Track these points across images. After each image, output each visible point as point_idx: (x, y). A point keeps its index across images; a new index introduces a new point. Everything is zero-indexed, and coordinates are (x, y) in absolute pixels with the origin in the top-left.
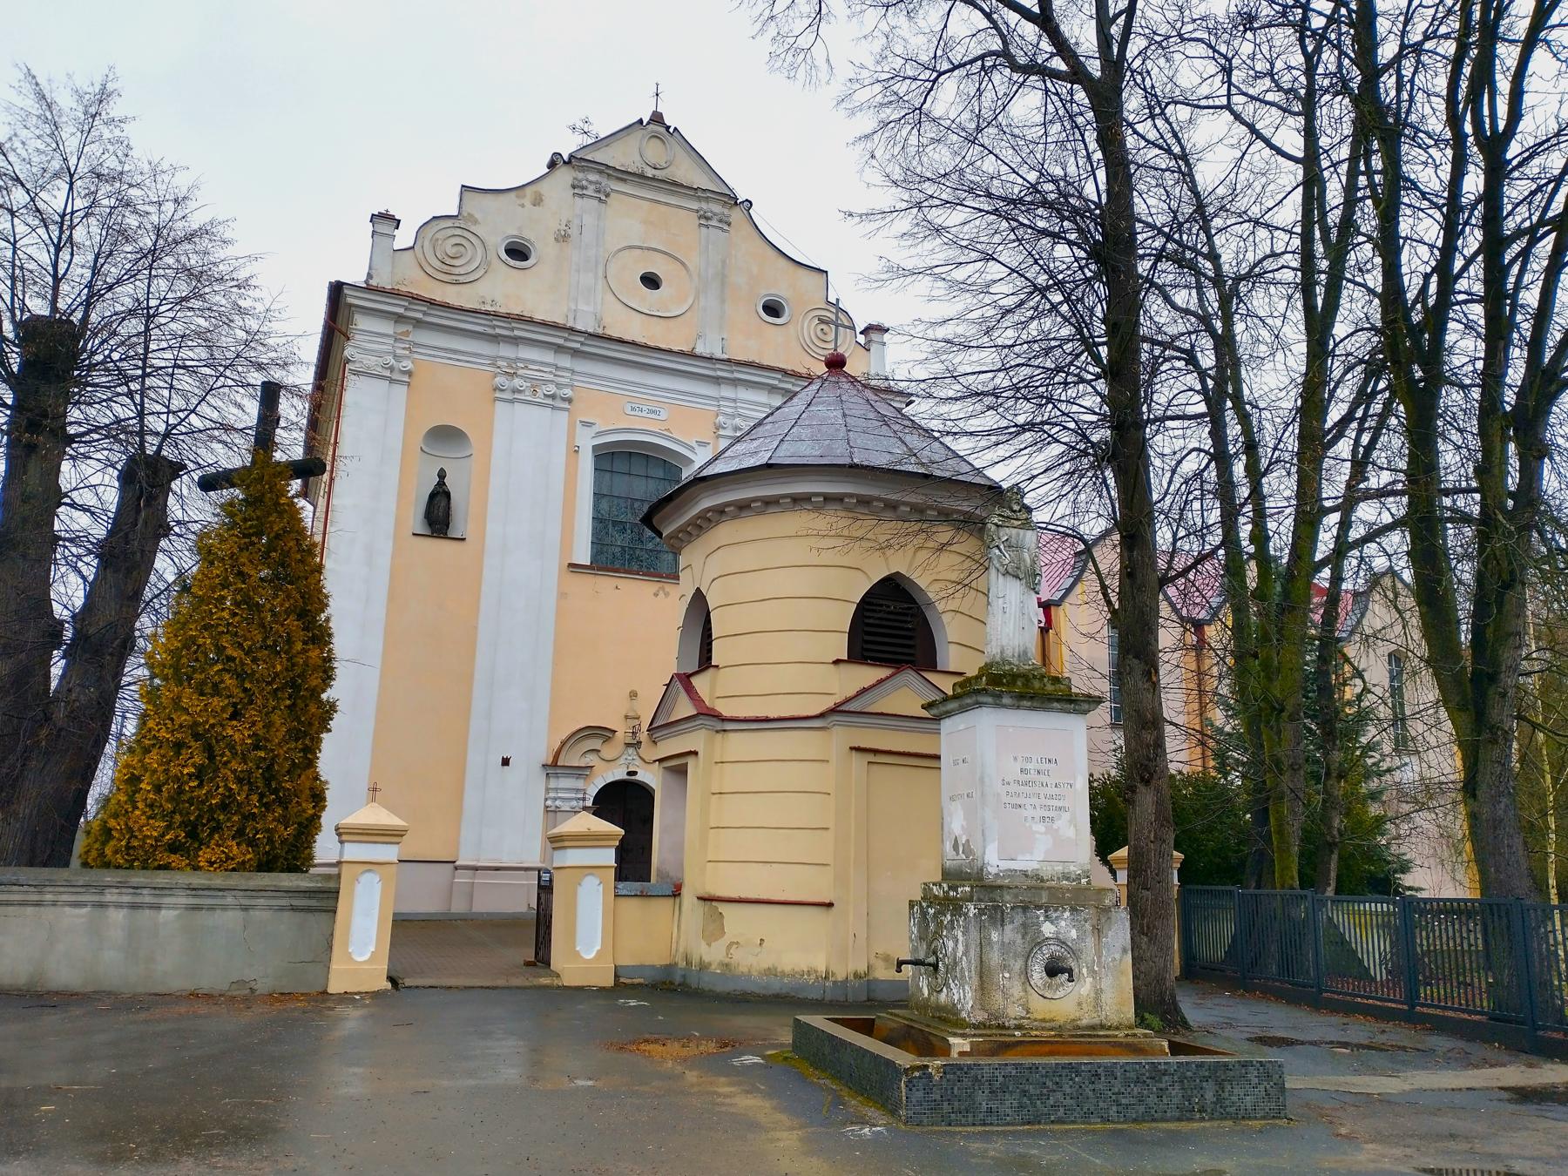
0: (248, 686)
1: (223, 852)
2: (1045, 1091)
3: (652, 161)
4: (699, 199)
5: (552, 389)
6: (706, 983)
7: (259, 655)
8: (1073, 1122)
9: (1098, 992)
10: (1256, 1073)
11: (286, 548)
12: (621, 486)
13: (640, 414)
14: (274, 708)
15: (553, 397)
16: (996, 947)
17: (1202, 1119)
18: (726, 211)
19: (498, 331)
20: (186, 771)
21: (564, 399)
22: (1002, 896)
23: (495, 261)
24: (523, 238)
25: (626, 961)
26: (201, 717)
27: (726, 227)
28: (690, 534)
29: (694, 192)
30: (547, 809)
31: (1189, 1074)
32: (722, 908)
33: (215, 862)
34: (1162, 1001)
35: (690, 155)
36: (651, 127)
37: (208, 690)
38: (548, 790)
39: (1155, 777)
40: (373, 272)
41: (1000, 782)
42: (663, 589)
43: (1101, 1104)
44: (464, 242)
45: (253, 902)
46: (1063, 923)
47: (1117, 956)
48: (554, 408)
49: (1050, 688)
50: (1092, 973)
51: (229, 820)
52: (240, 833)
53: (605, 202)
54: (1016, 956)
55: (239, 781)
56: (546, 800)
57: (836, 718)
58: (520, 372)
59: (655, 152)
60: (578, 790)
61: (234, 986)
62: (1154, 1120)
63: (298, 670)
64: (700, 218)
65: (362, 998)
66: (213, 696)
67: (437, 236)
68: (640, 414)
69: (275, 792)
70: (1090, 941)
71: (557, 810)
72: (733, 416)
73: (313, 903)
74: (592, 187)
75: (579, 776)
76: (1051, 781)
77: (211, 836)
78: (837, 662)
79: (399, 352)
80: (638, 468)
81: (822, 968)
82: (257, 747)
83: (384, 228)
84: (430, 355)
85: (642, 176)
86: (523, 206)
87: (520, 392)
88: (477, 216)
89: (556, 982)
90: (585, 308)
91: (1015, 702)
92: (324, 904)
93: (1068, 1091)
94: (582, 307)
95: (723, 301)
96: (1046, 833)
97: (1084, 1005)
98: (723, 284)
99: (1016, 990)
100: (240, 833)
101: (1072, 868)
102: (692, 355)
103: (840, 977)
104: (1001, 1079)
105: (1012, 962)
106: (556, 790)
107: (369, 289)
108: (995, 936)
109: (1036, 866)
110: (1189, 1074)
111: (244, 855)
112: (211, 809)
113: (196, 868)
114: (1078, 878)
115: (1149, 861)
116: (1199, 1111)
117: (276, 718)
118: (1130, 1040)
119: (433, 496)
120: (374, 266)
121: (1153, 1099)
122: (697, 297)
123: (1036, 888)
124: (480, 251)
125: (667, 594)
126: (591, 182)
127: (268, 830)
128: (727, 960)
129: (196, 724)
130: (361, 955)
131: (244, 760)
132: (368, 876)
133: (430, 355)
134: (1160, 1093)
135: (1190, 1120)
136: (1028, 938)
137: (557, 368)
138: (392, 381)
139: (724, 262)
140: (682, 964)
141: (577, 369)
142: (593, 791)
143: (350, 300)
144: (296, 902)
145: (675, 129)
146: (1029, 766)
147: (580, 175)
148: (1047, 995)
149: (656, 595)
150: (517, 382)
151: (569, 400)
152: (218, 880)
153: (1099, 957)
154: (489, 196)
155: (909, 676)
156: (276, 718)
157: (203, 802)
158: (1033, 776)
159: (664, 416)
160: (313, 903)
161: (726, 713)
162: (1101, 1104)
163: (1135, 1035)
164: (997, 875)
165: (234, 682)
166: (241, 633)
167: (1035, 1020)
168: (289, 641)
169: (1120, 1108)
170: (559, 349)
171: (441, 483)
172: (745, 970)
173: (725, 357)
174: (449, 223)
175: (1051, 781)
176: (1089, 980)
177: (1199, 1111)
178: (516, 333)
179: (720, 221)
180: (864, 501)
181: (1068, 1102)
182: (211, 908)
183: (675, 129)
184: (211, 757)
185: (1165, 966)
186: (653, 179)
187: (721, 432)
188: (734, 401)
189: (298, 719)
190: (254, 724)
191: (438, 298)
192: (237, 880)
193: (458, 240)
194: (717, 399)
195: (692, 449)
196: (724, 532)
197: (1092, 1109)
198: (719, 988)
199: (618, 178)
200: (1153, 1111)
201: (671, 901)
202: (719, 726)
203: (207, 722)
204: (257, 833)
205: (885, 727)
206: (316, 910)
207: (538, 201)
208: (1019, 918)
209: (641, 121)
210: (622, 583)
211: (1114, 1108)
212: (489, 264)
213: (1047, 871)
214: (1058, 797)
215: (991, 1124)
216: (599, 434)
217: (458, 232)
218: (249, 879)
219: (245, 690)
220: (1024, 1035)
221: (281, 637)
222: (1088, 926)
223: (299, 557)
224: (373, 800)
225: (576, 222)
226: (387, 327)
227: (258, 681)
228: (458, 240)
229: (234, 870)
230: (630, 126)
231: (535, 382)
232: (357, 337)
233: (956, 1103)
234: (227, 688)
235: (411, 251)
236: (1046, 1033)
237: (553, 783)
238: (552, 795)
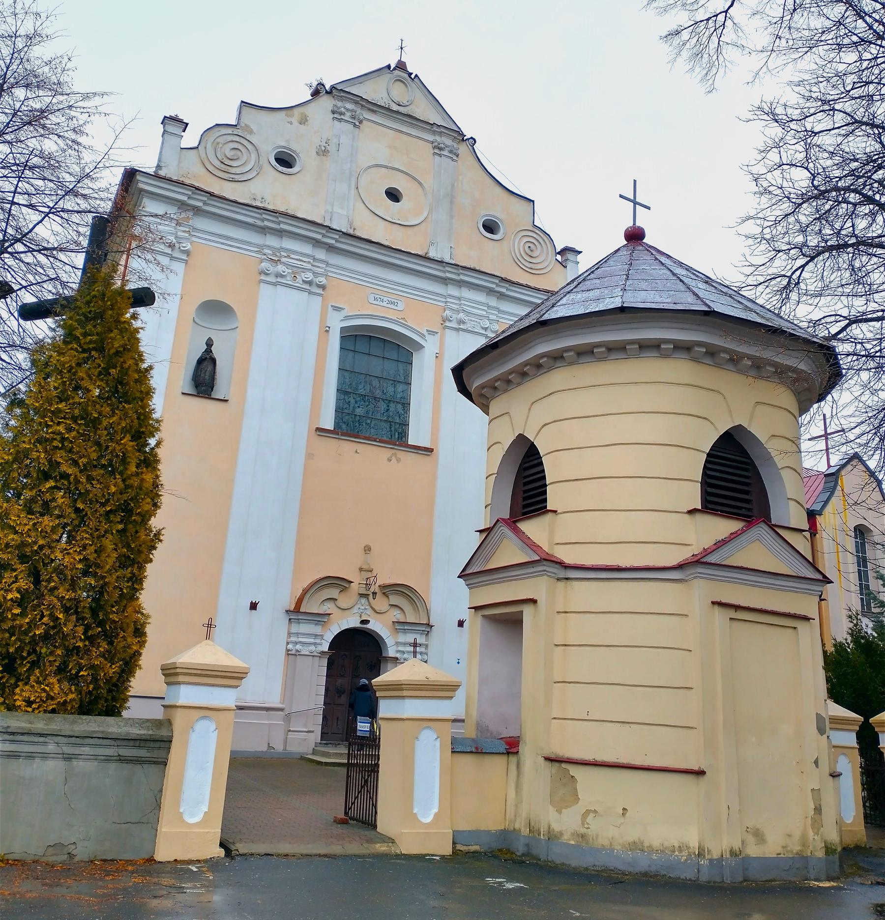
0: (80, 506)
1: (44, 690)
3: (396, 99)
4: (434, 133)
5: (310, 276)
6: (557, 856)
7: (94, 473)
11: (126, 366)
12: (362, 364)
13: (381, 303)
14: (106, 532)
15: (310, 283)
18: (455, 145)
19: (266, 223)
20: (10, 596)
21: (319, 286)
23: (266, 166)
24: (290, 149)
25: (464, 826)
26: (30, 536)
27: (455, 158)
28: (495, 388)
29: (430, 126)
30: (288, 653)
32: (574, 770)
33: (34, 702)
35: (427, 98)
36: (397, 72)
37: (37, 508)
38: (289, 634)
42: (395, 455)
44: (240, 147)
45: (77, 751)
48: (310, 293)
51: (52, 653)
52: (61, 670)
53: (358, 127)
55: (66, 610)
56: (288, 643)
57: (700, 570)
58: (283, 260)
59: (399, 93)
60: (316, 636)
61: (51, 849)
63: (131, 493)
64: (434, 148)
65: (201, 871)
66: (42, 515)
67: (218, 140)
68: (381, 303)
69: (101, 624)
71: (297, 654)
72: (458, 312)
73: (142, 753)
74: (348, 114)
75: (318, 623)
77: (30, 671)
78: (691, 512)
80: (376, 349)
81: (694, 844)
82: (86, 573)
83: (173, 128)
84: (206, 239)
85: (388, 109)
86: (291, 123)
87: (282, 276)
88: (254, 127)
89: (394, 850)
90: (340, 211)
92: (156, 754)
94: (337, 209)
95: (451, 217)
98: (452, 202)
100: (61, 670)
102: (426, 258)
103: (716, 855)
106: (297, 634)
107: (156, 176)
111: (67, 695)
112: (34, 641)
113: (11, 708)
117: (108, 543)
119: (200, 361)
120: (164, 159)
122: (430, 212)
124: (254, 156)
125: (398, 460)
126: (348, 110)
127: (92, 667)
128: (583, 831)
129: (23, 544)
131: (73, 586)
132: (204, 723)
133: (206, 239)
137: (315, 259)
139: (453, 186)
140: (525, 832)
141: (330, 262)
142: (329, 637)
143: (141, 186)
144: (125, 752)
145: (416, 76)
147: (339, 104)
149: (389, 460)
150: (280, 268)
151: (323, 287)
152: (40, 723)
154: (264, 113)
156: (108, 543)
157: (26, 633)
159: (401, 306)
160: (142, 753)
161: (568, 560)
165: (66, 501)
166: (76, 449)
168: (124, 461)
170: (317, 243)
171: (208, 351)
172: (606, 843)
173: (453, 262)
178: (283, 226)
179: (451, 152)
180: (712, 353)
182: (30, 756)
183: (416, 76)
184: (37, 582)
186: (397, 112)
187: (448, 324)
188: (459, 299)
189: (128, 546)
190: (84, 547)
191: (216, 192)
192: (61, 723)
193: (236, 145)
194: (445, 297)
195: (422, 336)
196: (559, 378)
198: (574, 862)
199: (370, 109)
201: (502, 760)
202: (562, 573)
203: (35, 543)
204: (81, 669)
205: (743, 582)
206: (145, 762)
207: (303, 121)
209: (389, 67)
210: (361, 448)
212: (261, 168)
216: (347, 318)
218: (74, 722)
219: (77, 510)
221: (117, 456)
223: (136, 376)
224: (208, 637)
225: (334, 141)
227: (91, 502)
228: (236, 145)
229: (53, 711)
230: (381, 69)
231: (295, 269)
234: (59, 507)
237: (295, 628)
238: (293, 639)
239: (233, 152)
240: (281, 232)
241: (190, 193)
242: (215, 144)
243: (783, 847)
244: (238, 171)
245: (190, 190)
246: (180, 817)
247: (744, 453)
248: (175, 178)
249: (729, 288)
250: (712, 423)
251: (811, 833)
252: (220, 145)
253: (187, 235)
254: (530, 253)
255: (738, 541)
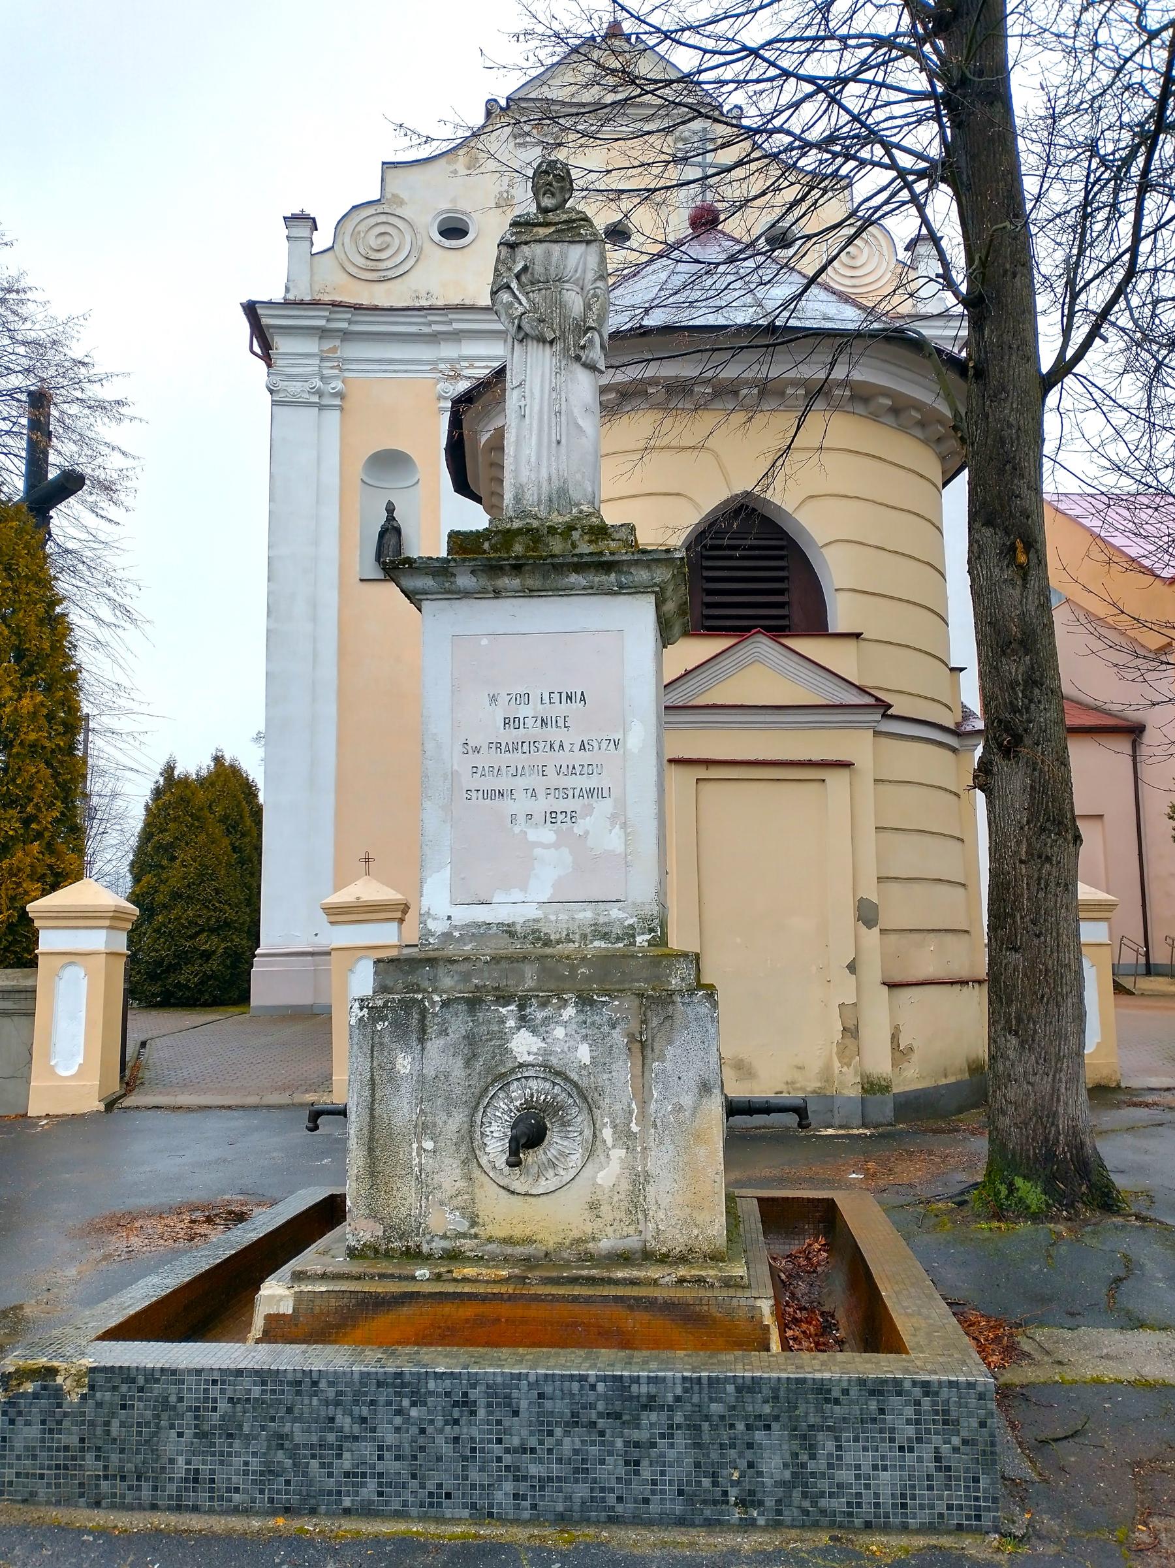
2: (331, 1438)
8: (399, 1515)
9: (639, 1181)
10: (909, 1412)
16: (405, 1087)
17: (748, 1525)
22: (433, 980)
23: (428, 246)
24: (457, 211)
31: (716, 1408)
34: (1050, 1156)
39: (1027, 741)
40: (291, 285)
41: (459, 748)
43: (474, 1476)
46: (559, 1032)
47: (687, 1100)
49: (584, 548)
50: (625, 1136)
54: (450, 1104)
62: (614, 1520)
67: (359, 228)
70: (623, 1070)
76: (571, 738)
79: (326, 372)
83: (302, 231)
88: (404, 195)
91: (484, 581)
93: (390, 1439)
96: (556, 845)
97: (605, 1209)
99: (449, 1177)
101: (615, 913)
104: (223, 1406)
105: (440, 1118)
107: (287, 303)
108: (404, 1064)
109: (532, 912)
110: (716, 1408)
114: (630, 934)
115: (1019, 896)
116: (742, 1503)
118: (687, 1294)
119: (382, 535)
121: (613, 1468)
123: (511, 959)
130: (67, 1069)
134: (635, 1454)
135: (710, 1524)
136: (479, 1065)
138: (322, 407)
146: (523, 711)
148: (517, 1186)
153: (644, 1104)
155: (762, 646)
158: (532, 731)
162: (474, 1476)
163: (700, 1280)
164: (447, 936)
167: (490, 1240)
169: (523, 1488)
171: (391, 518)
174: (371, 211)
175: (571, 738)
176: (618, 1154)
177: (742, 1503)
178: (456, 326)
180: (678, 389)
181: (389, 1465)
185: (1055, 1091)
193: (382, 229)
197: (449, 1485)
200: (611, 1499)
206: (14, 1014)
208: (459, 1025)
211: (509, 1486)
213: (557, 922)
214: (588, 770)
215: (195, 1509)
217: (383, 218)
220: (438, 1277)
222: (618, 1037)
226: (310, 346)
228: (382, 229)
232: (278, 362)
233: (114, 1458)
235: (330, 253)
236: (486, 1273)
239: (381, 239)
240: (457, 334)
241: (327, 314)
242: (354, 234)
243: (787, 1083)
244: (389, 264)
245: (326, 310)
246: (52, 1070)
247: (781, 533)
248: (307, 298)
249: (1163, 226)
250: (690, 499)
251: (836, 1064)
252: (362, 235)
253: (337, 371)
254: (852, 263)
255: (718, 667)
